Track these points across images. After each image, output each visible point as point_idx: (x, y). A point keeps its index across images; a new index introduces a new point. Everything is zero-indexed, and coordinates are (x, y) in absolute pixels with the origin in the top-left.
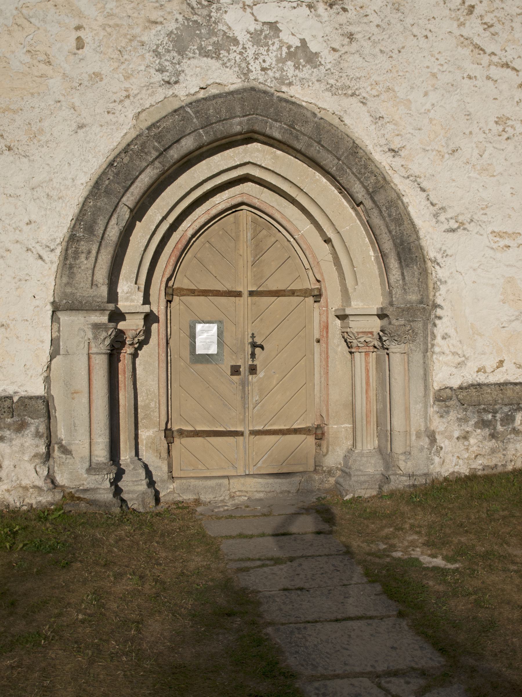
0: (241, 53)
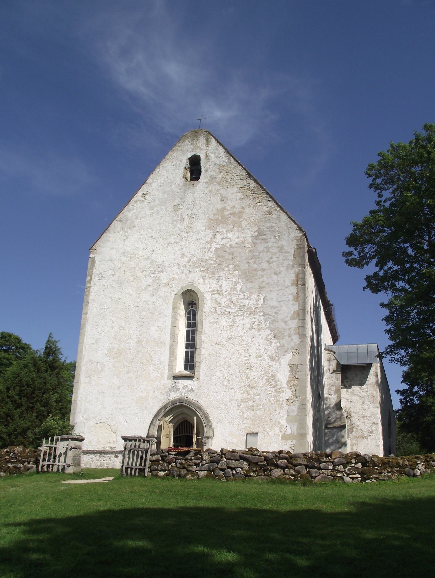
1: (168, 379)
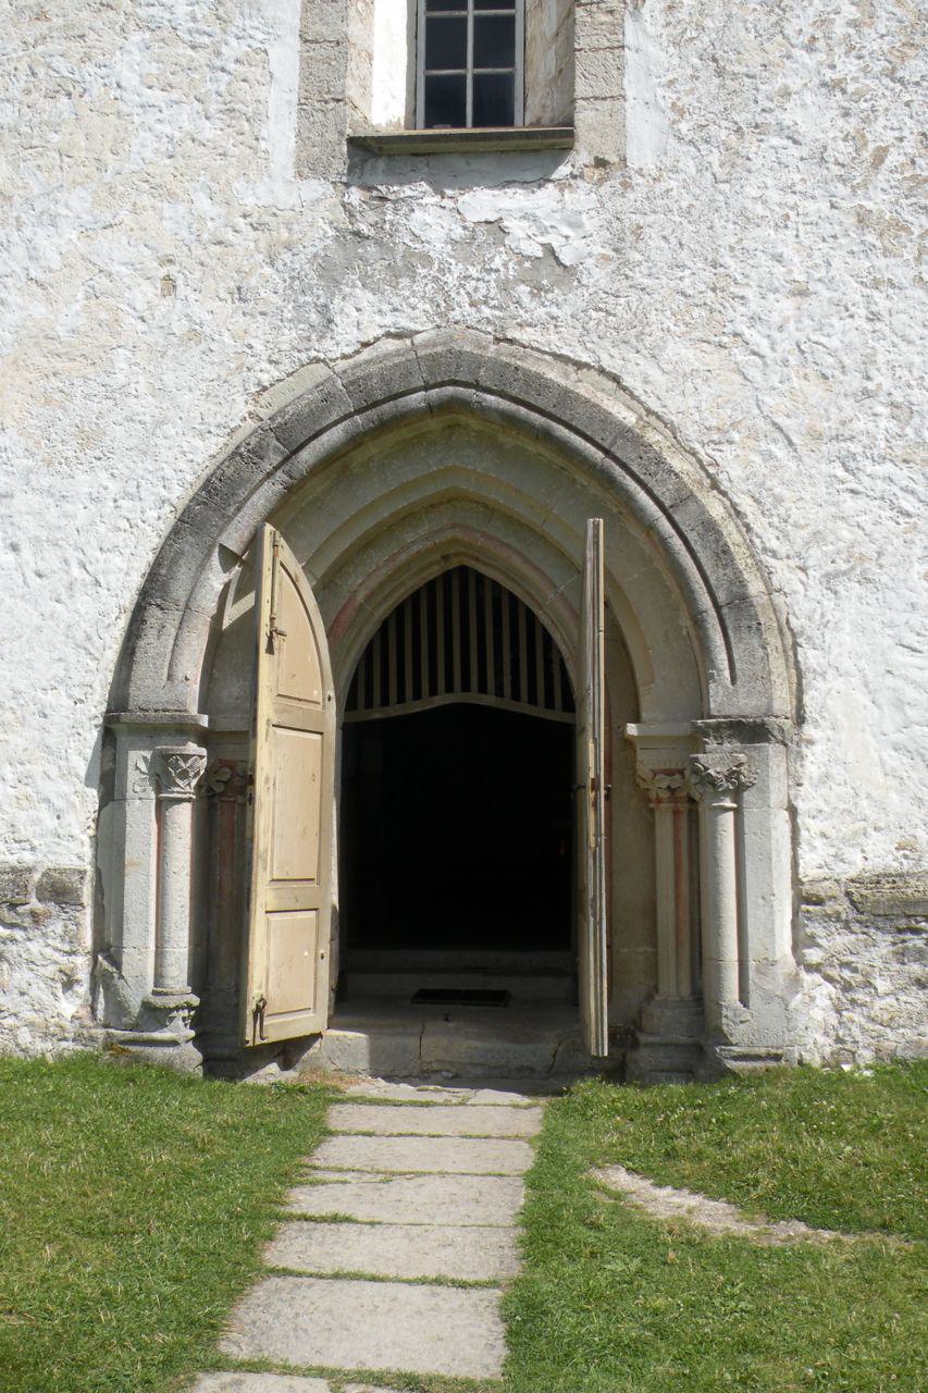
0: (436, 280)
1: (308, 167)
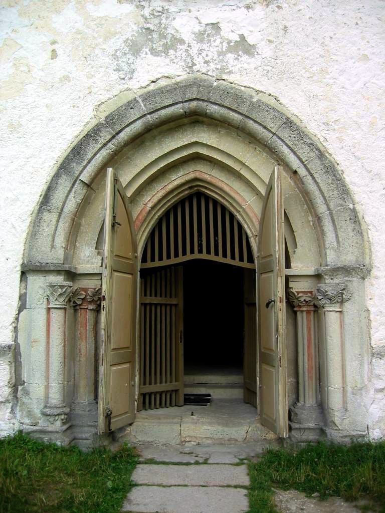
0: (187, 51)
